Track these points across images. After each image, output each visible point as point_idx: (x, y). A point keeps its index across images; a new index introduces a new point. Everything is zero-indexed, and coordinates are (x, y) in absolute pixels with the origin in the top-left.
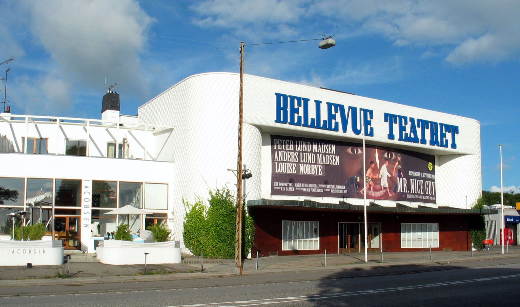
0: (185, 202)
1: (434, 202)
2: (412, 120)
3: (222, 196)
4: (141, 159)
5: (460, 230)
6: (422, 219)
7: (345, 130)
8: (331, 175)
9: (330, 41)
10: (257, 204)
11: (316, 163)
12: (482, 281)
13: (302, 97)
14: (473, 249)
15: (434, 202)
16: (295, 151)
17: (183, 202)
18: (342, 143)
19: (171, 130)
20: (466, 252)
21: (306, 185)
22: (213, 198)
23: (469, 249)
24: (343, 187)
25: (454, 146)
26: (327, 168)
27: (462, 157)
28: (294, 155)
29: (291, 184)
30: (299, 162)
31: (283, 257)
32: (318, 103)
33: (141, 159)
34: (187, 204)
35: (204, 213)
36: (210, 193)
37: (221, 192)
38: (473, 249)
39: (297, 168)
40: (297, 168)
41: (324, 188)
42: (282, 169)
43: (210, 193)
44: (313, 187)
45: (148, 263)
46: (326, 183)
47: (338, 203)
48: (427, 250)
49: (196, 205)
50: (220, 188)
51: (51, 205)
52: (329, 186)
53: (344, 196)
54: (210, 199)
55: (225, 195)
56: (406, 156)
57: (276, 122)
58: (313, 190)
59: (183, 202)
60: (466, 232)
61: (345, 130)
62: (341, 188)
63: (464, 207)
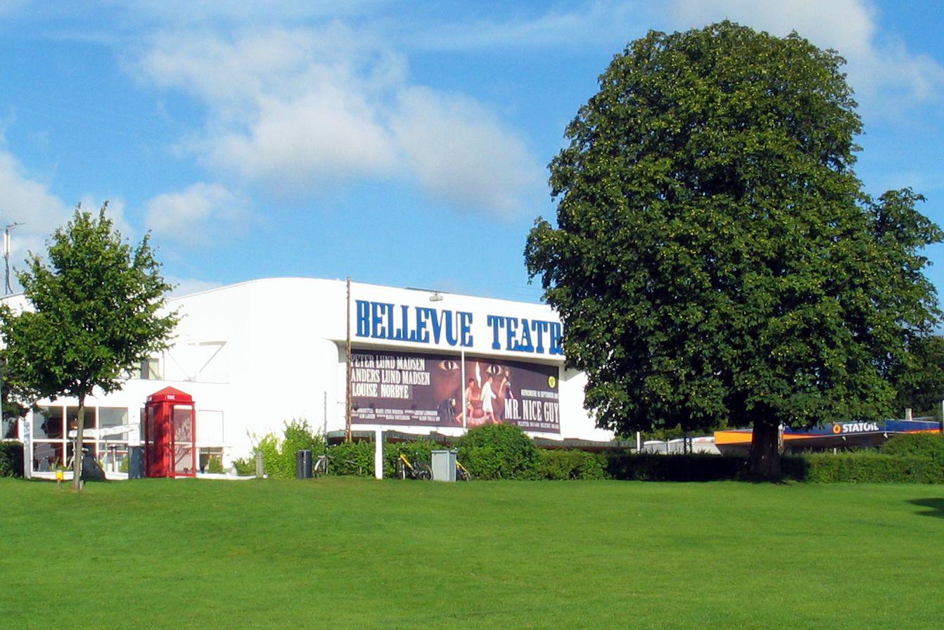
0: (251, 434)
3: (299, 427)
7: (437, 341)
11: (401, 383)
15: (557, 431)
16: (375, 369)
17: (248, 434)
18: (432, 357)
19: (223, 344)
21: (388, 411)
22: (289, 429)
24: (436, 413)
26: (415, 389)
29: (371, 411)
32: (405, 309)
36: (285, 422)
39: (379, 390)
40: (379, 390)
41: (411, 415)
44: (398, 414)
46: (414, 408)
49: (267, 437)
52: (417, 412)
54: (285, 430)
55: (302, 425)
56: (517, 369)
58: (397, 418)
59: (248, 434)
61: (437, 341)
62: (432, 414)
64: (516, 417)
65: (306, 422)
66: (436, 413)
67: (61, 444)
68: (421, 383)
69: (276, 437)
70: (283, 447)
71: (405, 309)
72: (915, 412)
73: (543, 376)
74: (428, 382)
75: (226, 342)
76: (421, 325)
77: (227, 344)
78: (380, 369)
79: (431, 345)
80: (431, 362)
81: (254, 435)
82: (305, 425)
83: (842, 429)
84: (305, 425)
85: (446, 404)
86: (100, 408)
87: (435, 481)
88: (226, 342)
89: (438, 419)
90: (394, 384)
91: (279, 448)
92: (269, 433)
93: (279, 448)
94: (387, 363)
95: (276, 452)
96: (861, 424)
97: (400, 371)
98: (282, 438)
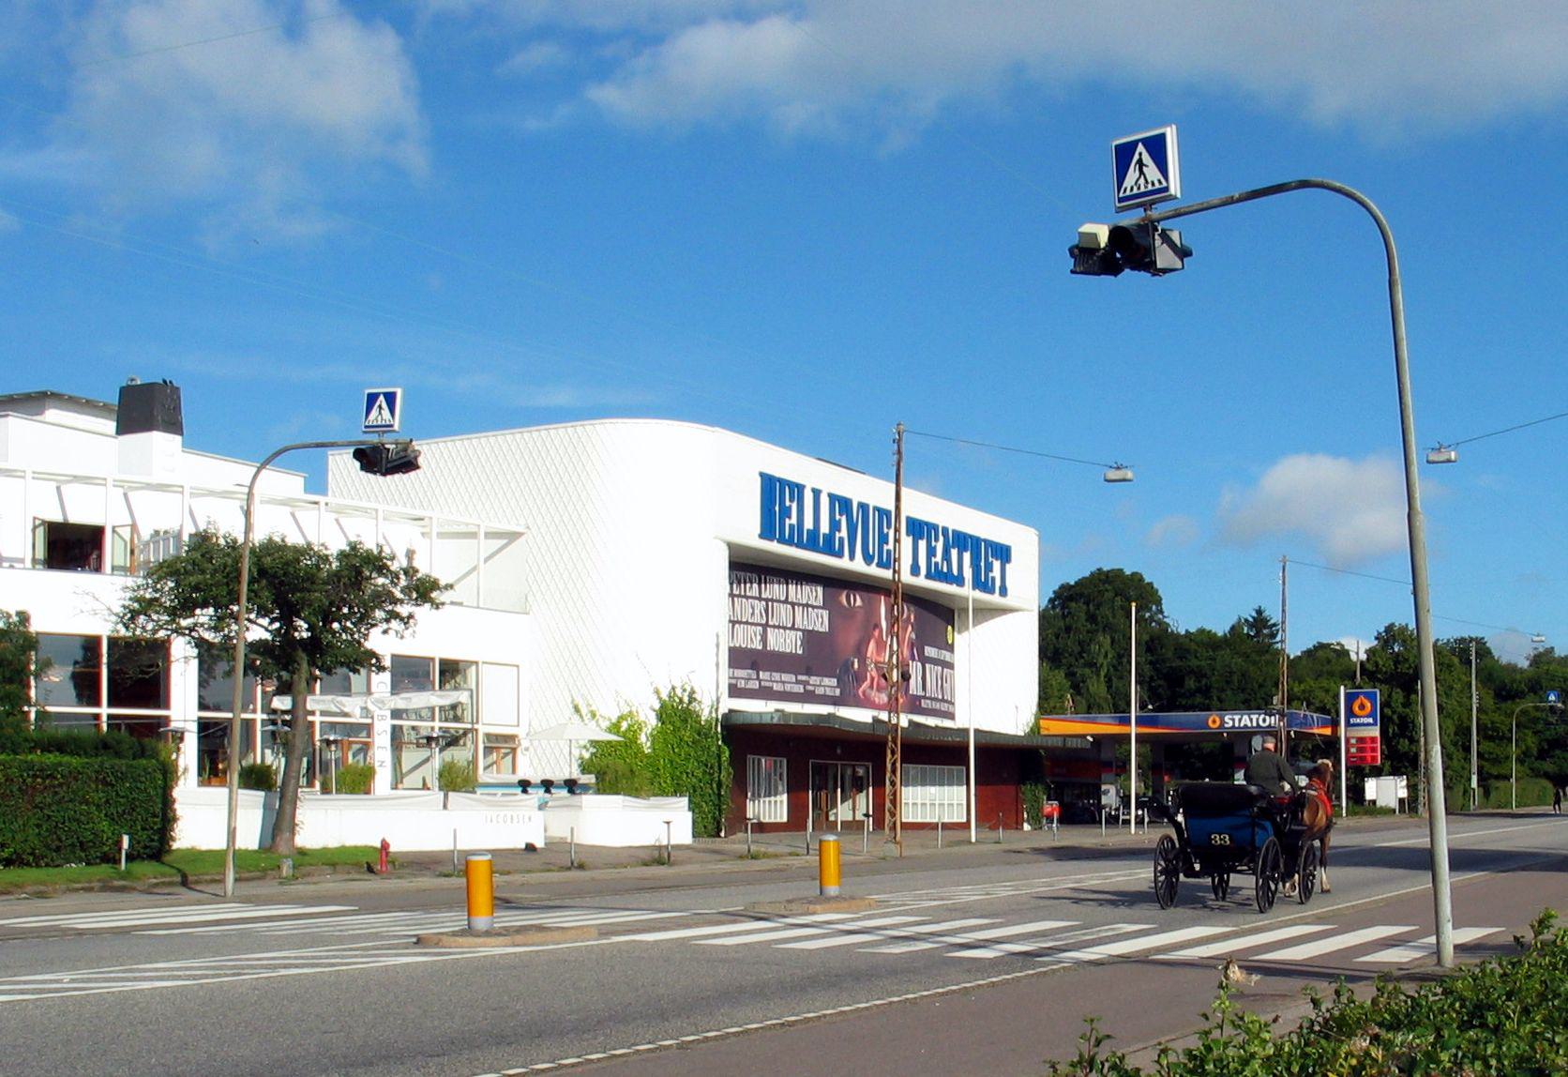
0: (584, 711)
1: (951, 716)
2: (945, 530)
3: (681, 701)
4: (461, 604)
5: (1004, 782)
6: (936, 754)
7: (852, 557)
8: (819, 655)
9: (1130, 475)
10: (767, 720)
11: (793, 628)
12: (492, 965)
13: (983, 536)
14: (1026, 827)
15: (951, 716)
16: (760, 599)
17: (577, 709)
18: (834, 582)
19: (513, 536)
20: (1012, 834)
21: (776, 676)
22: (663, 705)
23: (1018, 826)
24: (834, 682)
25: (1003, 592)
26: (810, 636)
27: (1010, 616)
28: (760, 606)
29: (753, 673)
30: (765, 626)
31: (764, 835)
32: (817, 493)
33: (461, 604)
34: (594, 715)
35: (643, 739)
36: (657, 692)
37: (679, 692)
38: (1026, 827)
39: (764, 640)
40: (764, 640)
41: (805, 683)
42: (740, 642)
43: (657, 692)
44: (787, 681)
45: (673, 842)
46: (809, 672)
47: (870, 720)
48: (933, 827)
49: (621, 718)
50: (678, 685)
51: (231, 710)
52: (814, 680)
53: (835, 702)
54: (657, 706)
55: (686, 699)
56: (925, 613)
57: (761, 536)
58: (788, 688)
59: (577, 709)
60: (1012, 789)
61: (852, 557)
62: (828, 685)
63: (1012, 732)
64: (920, 693)
65: (693, 692)
66: (834, 682)
67: (111, 704)
68: (819, 628)
69: (642, 718)
70: (654, 738)
71: (817, 493)
72: (1205, 692)
73: (940, 623)
74: (825, 628)
75: (520, 534)
76: (835, 526)
77: (522, 539)
78: (767, 600)
79: (843, 563)
80: (830, 590)
81: (594, 715)
82: (692, 699)
83: (1223, 722)
84: (692, 699)
85: (847, 666)
86: (394, 656)
87: (677, 792)
88: (520, 534)
89: (838, 692)
90: (785, 628)
91: (644, 741)
92: (626, 711)
93: (644, 741)
94: (776, 590)
95: (640, 748)
96: (1254, 717)
97: (793, 605)
98: (651, 721)
